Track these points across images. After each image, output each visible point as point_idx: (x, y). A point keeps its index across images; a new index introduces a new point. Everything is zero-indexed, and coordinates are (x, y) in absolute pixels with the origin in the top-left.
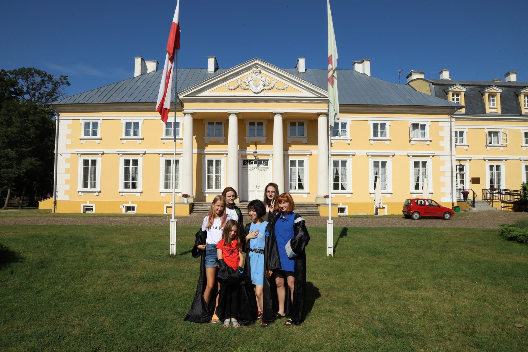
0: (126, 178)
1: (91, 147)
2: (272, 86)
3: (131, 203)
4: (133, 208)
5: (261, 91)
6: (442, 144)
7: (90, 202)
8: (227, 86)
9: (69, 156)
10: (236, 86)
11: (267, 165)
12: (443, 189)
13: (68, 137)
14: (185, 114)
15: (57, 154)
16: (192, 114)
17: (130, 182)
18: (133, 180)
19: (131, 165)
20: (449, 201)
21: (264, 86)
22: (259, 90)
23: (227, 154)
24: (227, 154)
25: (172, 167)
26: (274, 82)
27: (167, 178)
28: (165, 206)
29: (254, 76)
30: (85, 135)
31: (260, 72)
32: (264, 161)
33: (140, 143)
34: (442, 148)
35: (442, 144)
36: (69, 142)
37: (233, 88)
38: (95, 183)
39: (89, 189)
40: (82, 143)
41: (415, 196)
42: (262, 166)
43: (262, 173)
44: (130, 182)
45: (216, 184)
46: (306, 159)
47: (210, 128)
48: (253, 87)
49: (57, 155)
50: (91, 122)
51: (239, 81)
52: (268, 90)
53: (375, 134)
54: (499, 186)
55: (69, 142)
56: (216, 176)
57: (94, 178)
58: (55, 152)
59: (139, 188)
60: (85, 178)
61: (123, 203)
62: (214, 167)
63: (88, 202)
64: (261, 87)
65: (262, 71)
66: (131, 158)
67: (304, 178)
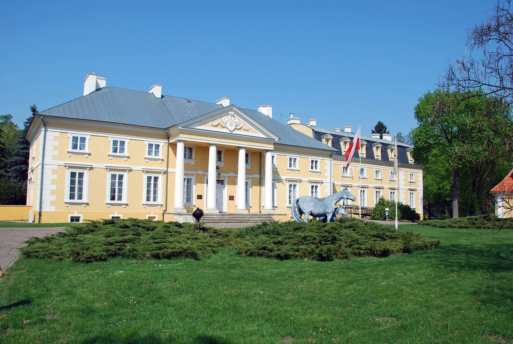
4: (78, 219)
6: (326, 174)
9: (56, 167)
10: (217, 124)
25: (314, 188)
34: (326, 177)
35: (326, 174)
36: (56, 153)
37: (215, 125)
38: (147, 194)
47: (195, 153)
48: (228, 125)
53: (75, 147)
54: (316, 196)
55: (56, 153)
57: (81, 190)
60: (72, 189)
61: (69, 213)
64: (234, 127)
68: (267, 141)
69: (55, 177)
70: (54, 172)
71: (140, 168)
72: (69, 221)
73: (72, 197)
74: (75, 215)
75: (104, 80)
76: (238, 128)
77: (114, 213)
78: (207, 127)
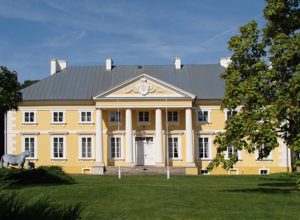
0: (55, 150)
1: (30, 129)
2: (154, 90)
3: (265, 168)
4: (265, 172)
5: (147, 94)
7: (266, 168)
8: (124, 90)
9: (15, 135)
10: (130, 91)
11: (152, 141)
12: (280, 157)
13: (14, 122)
14: (97, 109)
15: (6, 134)
16: (101, 109)
17: (58, 153)
18: (60, 151)
19: (58, 142)
20: (285, 166)
21: (149, 90)
22: (145, 93)
23: (95, 134)
24: (95, 134)
26: (155, 87)
27: (84, 150)
28: (83, 169)
29: (142, 84)
30: (26, 121)
31: (146, 81)
32: (150, 138)
33: (64, 127)
36: (15, 125)
37: (128, 92)
38: (34, 154)
39: (87, 158)
40: (81, 127)
41: (55, 164)
42: (150, 142)
43: (149, 146)
44: (58, 153)
45: (118, 154)
46: (121, 137)
47: (113, 118)
49: (6, 135)
50: (29, 112)
51: (132, 87)
52: (152, 93)
55: (15, 125)
56: (205, 149)
58: (5, 133)
59: (64, 157)
62: (203, 142)
63: (87, 167)
64: (147, 91)
65: (148, 80)
66: (58, 137)
67: (178, 150)
68: (186, 99)
69: (15, 142)
70: (14, 138)
71: (75, 132)
72: (260, 173)
73: (84, 155)
74: (264, 169)
75: (64, 62)
76: (150, 91)
77: (262, 168)
78: (106, 97)
